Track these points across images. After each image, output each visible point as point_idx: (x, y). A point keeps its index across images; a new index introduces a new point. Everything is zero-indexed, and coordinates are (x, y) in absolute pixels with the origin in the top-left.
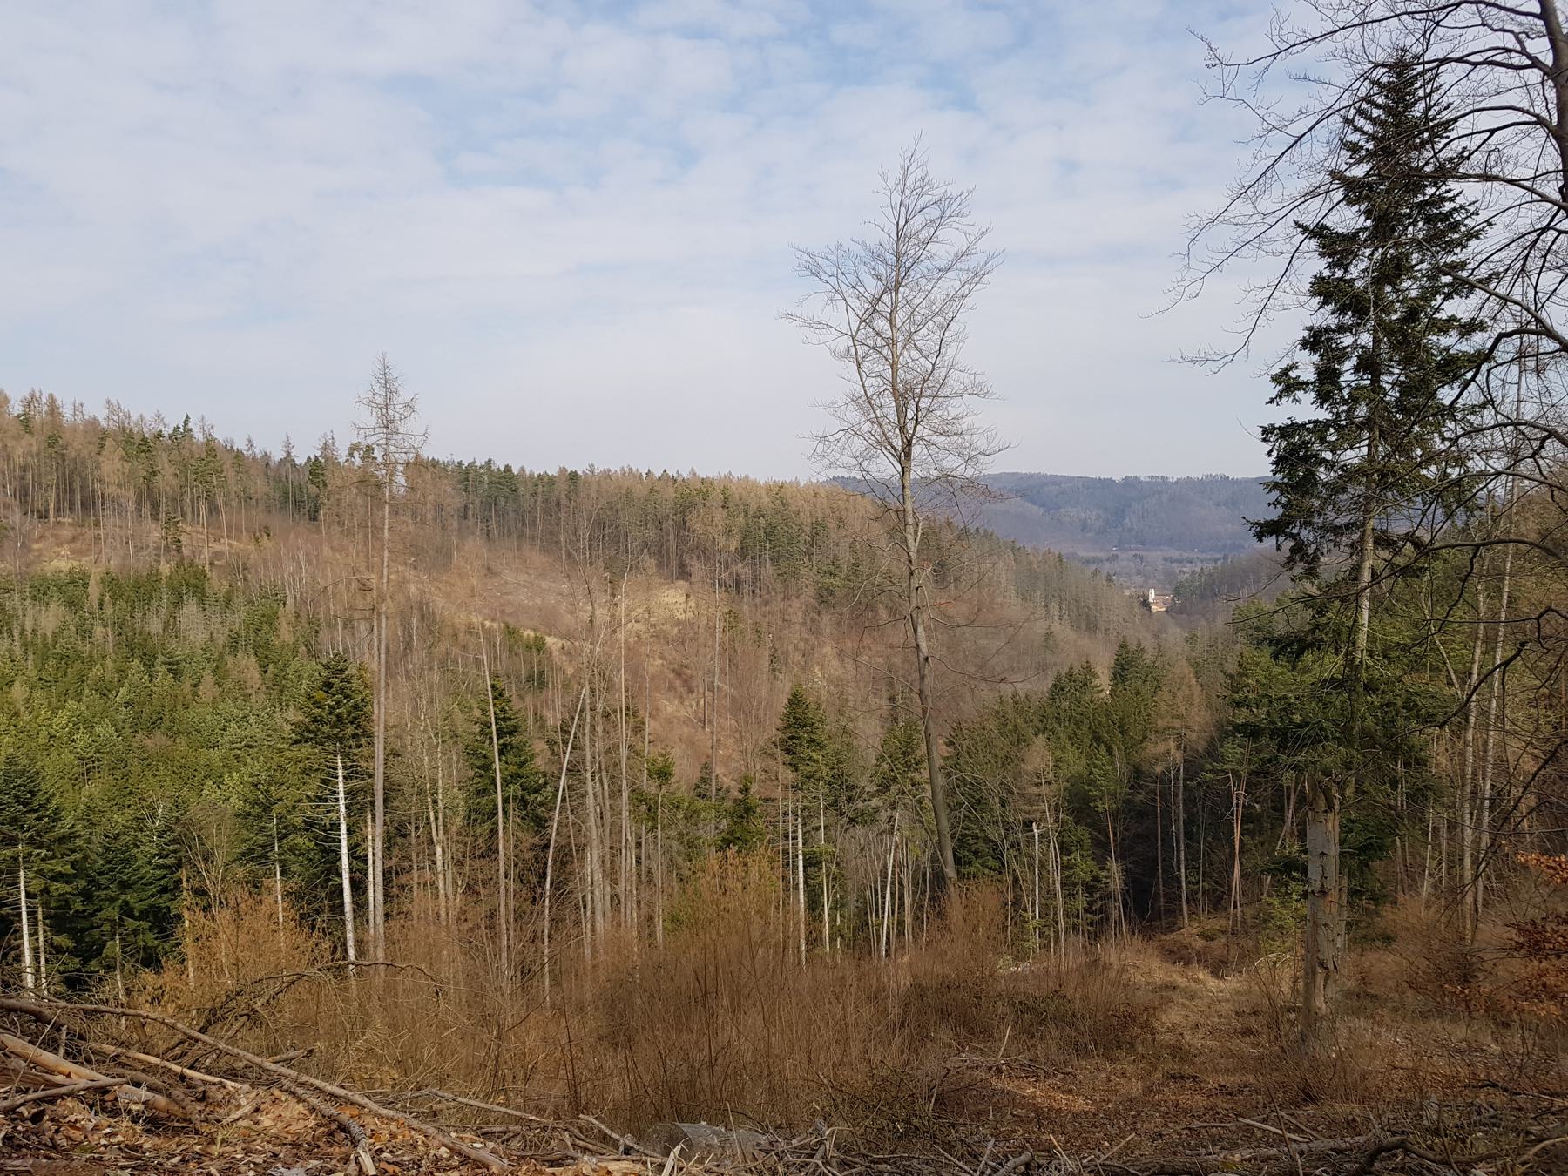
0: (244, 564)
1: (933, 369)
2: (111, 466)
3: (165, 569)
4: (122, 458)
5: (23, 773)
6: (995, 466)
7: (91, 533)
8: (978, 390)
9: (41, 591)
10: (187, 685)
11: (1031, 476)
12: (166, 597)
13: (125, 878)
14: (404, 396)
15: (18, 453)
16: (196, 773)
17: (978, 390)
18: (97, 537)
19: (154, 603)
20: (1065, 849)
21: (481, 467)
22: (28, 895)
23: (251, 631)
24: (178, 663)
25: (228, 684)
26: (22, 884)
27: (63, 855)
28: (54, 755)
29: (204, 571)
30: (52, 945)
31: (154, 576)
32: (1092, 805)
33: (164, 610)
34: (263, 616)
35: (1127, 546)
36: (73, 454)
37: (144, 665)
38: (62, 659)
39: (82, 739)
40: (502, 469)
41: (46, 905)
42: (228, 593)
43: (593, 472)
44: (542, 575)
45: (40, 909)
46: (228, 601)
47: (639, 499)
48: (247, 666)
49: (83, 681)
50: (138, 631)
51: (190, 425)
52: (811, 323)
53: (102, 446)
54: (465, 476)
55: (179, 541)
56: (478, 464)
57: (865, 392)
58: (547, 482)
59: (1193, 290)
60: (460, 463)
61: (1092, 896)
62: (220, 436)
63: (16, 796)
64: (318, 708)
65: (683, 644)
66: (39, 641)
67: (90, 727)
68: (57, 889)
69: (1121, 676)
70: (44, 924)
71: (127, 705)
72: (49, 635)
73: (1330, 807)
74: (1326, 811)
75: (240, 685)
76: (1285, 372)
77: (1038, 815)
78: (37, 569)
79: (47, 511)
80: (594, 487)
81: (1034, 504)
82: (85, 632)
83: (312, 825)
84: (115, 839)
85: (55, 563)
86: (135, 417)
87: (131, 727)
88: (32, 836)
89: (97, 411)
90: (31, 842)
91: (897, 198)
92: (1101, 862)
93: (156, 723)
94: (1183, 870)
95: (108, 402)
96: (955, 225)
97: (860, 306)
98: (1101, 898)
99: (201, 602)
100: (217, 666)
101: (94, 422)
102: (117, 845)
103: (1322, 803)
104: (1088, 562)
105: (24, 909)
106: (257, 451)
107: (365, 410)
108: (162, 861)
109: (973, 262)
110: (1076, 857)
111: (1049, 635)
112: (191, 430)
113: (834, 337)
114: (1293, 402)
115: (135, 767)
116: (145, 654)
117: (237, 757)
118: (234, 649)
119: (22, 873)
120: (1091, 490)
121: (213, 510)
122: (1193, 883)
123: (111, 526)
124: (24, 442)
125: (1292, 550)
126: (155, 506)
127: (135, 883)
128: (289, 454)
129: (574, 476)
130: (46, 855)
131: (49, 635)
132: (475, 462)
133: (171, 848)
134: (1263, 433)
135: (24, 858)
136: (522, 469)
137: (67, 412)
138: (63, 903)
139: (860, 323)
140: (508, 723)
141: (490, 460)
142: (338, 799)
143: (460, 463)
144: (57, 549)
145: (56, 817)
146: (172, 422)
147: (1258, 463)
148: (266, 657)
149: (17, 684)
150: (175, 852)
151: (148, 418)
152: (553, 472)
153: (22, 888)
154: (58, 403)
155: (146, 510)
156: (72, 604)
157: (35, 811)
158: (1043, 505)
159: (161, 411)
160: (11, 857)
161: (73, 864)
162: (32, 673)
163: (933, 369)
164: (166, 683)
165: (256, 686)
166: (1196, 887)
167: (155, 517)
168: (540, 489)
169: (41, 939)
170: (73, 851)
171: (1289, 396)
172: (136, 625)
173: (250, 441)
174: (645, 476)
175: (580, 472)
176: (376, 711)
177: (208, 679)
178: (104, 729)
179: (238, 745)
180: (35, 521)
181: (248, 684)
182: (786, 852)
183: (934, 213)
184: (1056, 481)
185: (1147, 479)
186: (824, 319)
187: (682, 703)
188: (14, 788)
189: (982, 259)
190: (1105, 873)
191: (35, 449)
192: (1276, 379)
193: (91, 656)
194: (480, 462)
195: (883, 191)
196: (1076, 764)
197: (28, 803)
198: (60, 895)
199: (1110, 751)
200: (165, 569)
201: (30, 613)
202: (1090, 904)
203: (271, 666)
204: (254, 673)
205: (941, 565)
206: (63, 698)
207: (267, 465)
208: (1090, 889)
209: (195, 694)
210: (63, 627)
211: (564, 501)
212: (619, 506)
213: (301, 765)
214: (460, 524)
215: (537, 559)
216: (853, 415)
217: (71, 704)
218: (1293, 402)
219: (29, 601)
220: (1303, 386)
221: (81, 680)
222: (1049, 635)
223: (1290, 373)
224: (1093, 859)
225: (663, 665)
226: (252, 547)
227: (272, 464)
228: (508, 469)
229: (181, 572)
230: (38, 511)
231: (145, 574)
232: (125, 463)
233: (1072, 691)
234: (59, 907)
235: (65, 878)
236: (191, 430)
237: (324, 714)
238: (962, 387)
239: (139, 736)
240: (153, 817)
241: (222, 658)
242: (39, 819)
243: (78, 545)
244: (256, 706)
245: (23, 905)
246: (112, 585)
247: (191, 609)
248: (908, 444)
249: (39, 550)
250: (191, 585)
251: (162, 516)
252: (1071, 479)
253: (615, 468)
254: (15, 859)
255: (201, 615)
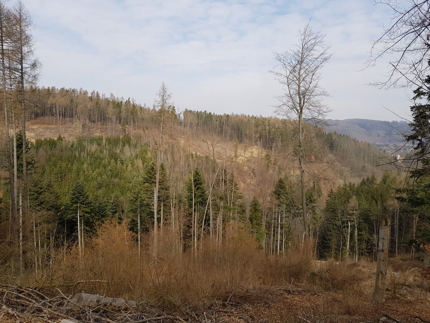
0: (140, 136)
1: (309, 87)
2: (110, 110)
3: (121, 137)
4: (113, 108)
5: (80, 186)
6: (328, 117)
7: (105, 126)
8: (324, 94)
9: (92, 141)
10: (125, 166)
11: (363, 120)
12: (121, 143)
13: (103, 214)
14: (168, 93)
15: (89, 106)
16: (125, 189)
17: (324, 94)
18: (106, 128)
19: (118, 145)
20: (359, 230)
21: (203, 113)
22: (80, 216)
23: (141, 154)
24: (123, 161)
25: (135, 167)
26: (78, 213)
27: (88, 207)
28: (92, 182)
29: (130, 137)
30: (85, 229)
31: (118, 139)
32: (369, 218)
33: (120, 147)
34: (144, 150)
35: (392, 142)
36: (101, 107)
37: (115, 161)
38: (96, 158)
39: (99, 179)
40: (209, 113)
41: (84, 219)
42: (136, 143)
43: (233, 115)
44: (218, 142)
45: (83, 220)
46: (136, 145)
47: (245, 123)
48: (139, 162)
49: (100, 164)
50: (114, 152)
51: (130, 100)
52: (277, 74)
53: (108, 105)
54: (199, 115)
55: (125, 130)
56: (202, 112)
57: (290, 93)
58: (220, 117)
59: (373, 63)
60: (198, 111)
61: (368, 244)
62: (137, 103)
63: (78, 192)
64: (150, 174)
65: (255, 163)
66: (91, 153)
67: (101, 176)
68: (86, 215)
69: (385, 180)
70: (83, 224)
71: (110, 171)
72: (93, 152)
73: (387, 224)
74: (385, 225)
75: (138, 167)
76: (418, 89)
77: (352, 219)
78: (91, 136)
79: (95, 121)
80: (233, 119)
81: (363, 128)
82: (102, 152)
83: (148, 205)
84: (101, 204)
85: (96, 134)
86: (116, 98)
87: (111, 176)
88: (81, 202)
89: (108, 96)
90: (81, 203)
91: (303, 37)
92: (371, 235)
93: (117, 176)
94: (397, 240)
95: (111, 94)
96: (320, 45)
97: (290, 68)
98: (371, 245)
99: (129, 146)
100: (132, 162)
101: (107, 99)
102: (101, 206)
103: (384, 222)
104: (379, 146)
105: (79, 220)
106: (147, 107)
107: (158, 96)
108: (112, 211)
109: (325, 56)
110: (363, 233)
111: (364, 167)
112: (130, 101)
113: (283, 78)
114: (419, 99)
115: (111, 187)
116: (115, 158)
117: (136, 186)
118: (137, 158)
119: (79, 211)
120: (381, 125)
121: (134, 122)
122: (400, 244)
123: (109, 125)
124: (90, 103)
125: (419, 144)
126: (120, 120)
127: (105, 216)
128: (154, 108)
129: (228, 116)
130: (85, 207)
131: (93, 152)
132: (201, 111)
133: (114, 207)
134: (411, 108)
135: (79, 207)
136: (214, 113)
137: (101, 96)
138: (88, 219)
139: (290, 74)
140: (199, 181)
141: (206, 111)
142: (154, 198)
143: (198, 111)
144: (97, 130)
145: (87, 198)
146: (125, 99)
147: (410, 118)
148: (144, 160)
149: (85, 164)
150: (115, 208)
151: (119, 98)
152: (222, 114)
153: (78, 214)
154: (99, 94)
155: (118, 122)
156: (99, 145)
157: (82, 196)
158: (365, 129)
159: (123, 96)
160: (76, 207)
161: (91, 209)
162: (88, 161)
163: (309, 87)
164: (120, 166)
165: (141, 168)
166: (401, 245)
167: (120, 123)
168: (218, 119)
169: (83, 228)
170: (91, 206)
171: (419, 97)
172: (114, 151)
173: (145, 104)
174: (247, 116)
175: (230, 115)
176: (157, 176)
177: (130, 165)
178: (104, 176)
179: (136, 183)
180: (92, 123)
181: (139, 167)
182: (274, 223)
183: (313, 42)
184: (371, 121)
185: (400, 122)
186: (280, 72)
187: (253, 180)
188: (78, 189)
189: (329, 55)
190: (372, 238)
191: (92, 105)
192: (415, 92)
193: (103, 158)
194: (203, 111)
195: (300, 35)
196: (365, 205)
197: (81, 194)
198: (87, 217)
199: (377, 203)
200: (121, 137)
201: (89, 146)
202: (367, 247)
203: (145, 163)
204: (141, 164)
205: (331, 144)
206: (95, 168)
207: (149, 110)
208: (367, 242)
209: (126, 169)
210: (97, 150)
211: (225, 123)
212: (239, 124)
213: (145, 189)
214: (197, 127)
215: (217, 138)
216: (285, 100)
217: (97, 170)
218: (419, 99)
219: (89, 143)
220: (424, 94)
221: (100, 164)
222: (364, 167)
223: (420, 90)
224: (369, 234)
225: (248, 169)
226: (143, 132)
227: (150, 110)
228: (210, 113)
229: (125, 138)
230: (93, 121)
231: (116, 138)
232: (113, 109)
233: (368, 184)
234: (87, 220)
235: (89, 213)
236: (130, 101)
237: (152, 176)
238: (320, 93)
239: (113, 179)
240: (111, 199)
241: (134, 160)
242: (83, 197)
243: (102, 130)
244: (141, 173)
245: (79, 218)
246: (109, 141)
247: (127, 147)
248: (301, 109)
249: (93, 131)
250: (127, 141)
251: (122, 123)
252: (375, 121)
253: (239, 114)
254: (77, 207)
255: (129, 149)
